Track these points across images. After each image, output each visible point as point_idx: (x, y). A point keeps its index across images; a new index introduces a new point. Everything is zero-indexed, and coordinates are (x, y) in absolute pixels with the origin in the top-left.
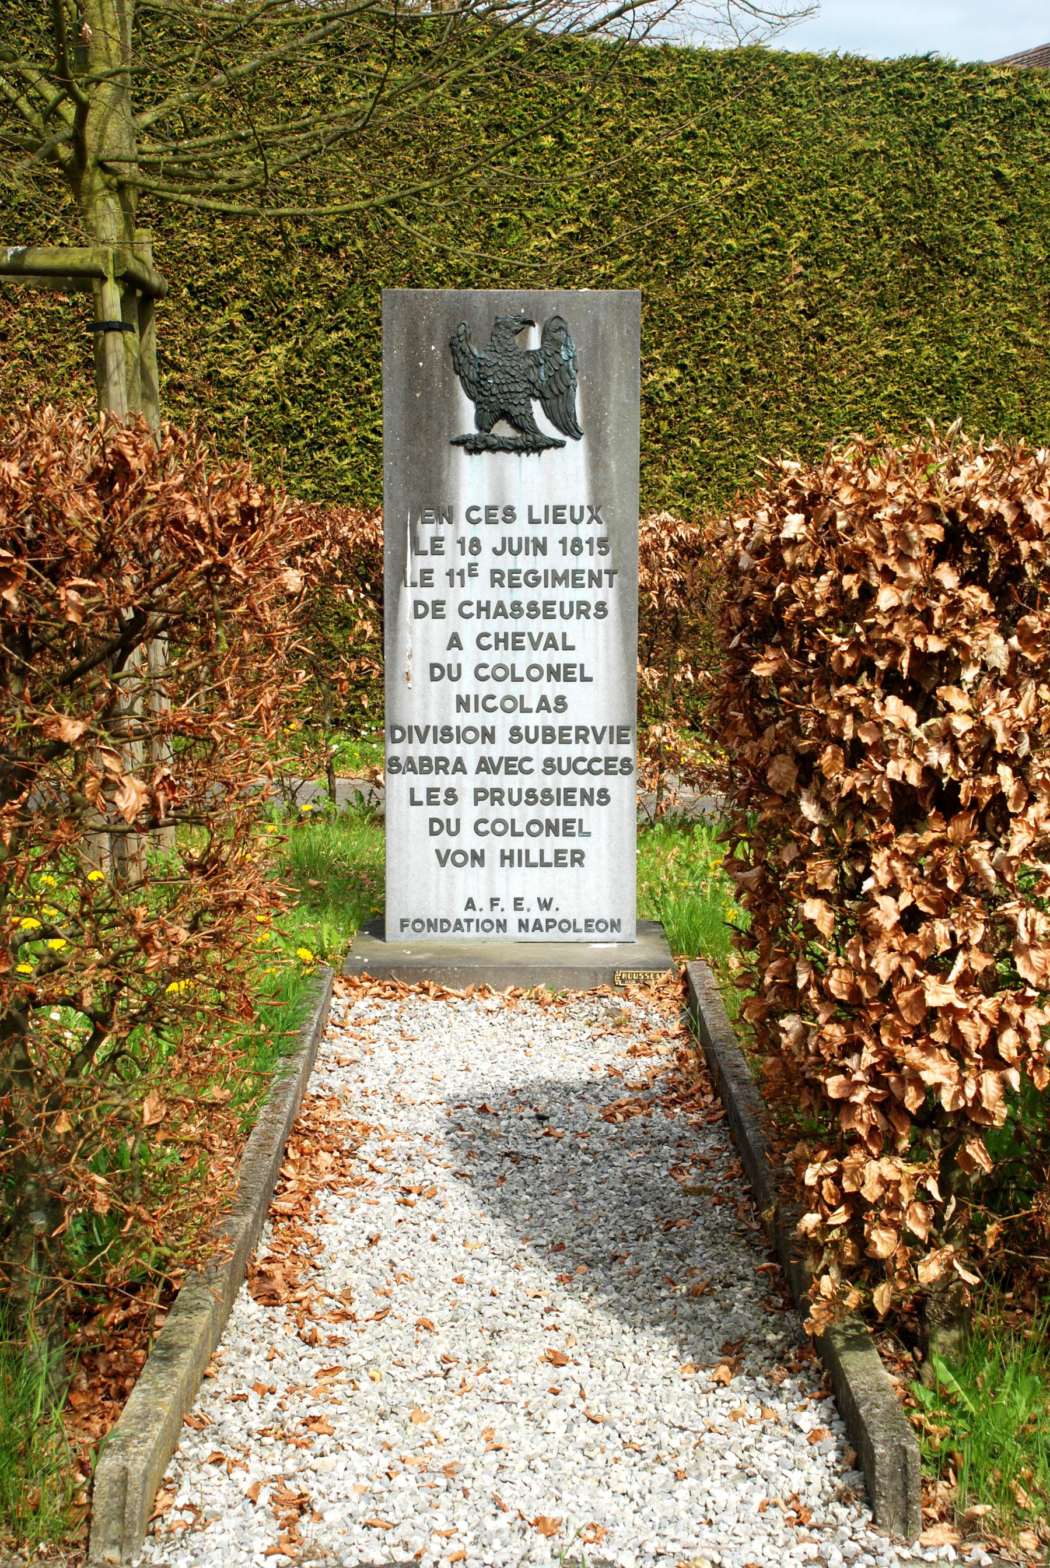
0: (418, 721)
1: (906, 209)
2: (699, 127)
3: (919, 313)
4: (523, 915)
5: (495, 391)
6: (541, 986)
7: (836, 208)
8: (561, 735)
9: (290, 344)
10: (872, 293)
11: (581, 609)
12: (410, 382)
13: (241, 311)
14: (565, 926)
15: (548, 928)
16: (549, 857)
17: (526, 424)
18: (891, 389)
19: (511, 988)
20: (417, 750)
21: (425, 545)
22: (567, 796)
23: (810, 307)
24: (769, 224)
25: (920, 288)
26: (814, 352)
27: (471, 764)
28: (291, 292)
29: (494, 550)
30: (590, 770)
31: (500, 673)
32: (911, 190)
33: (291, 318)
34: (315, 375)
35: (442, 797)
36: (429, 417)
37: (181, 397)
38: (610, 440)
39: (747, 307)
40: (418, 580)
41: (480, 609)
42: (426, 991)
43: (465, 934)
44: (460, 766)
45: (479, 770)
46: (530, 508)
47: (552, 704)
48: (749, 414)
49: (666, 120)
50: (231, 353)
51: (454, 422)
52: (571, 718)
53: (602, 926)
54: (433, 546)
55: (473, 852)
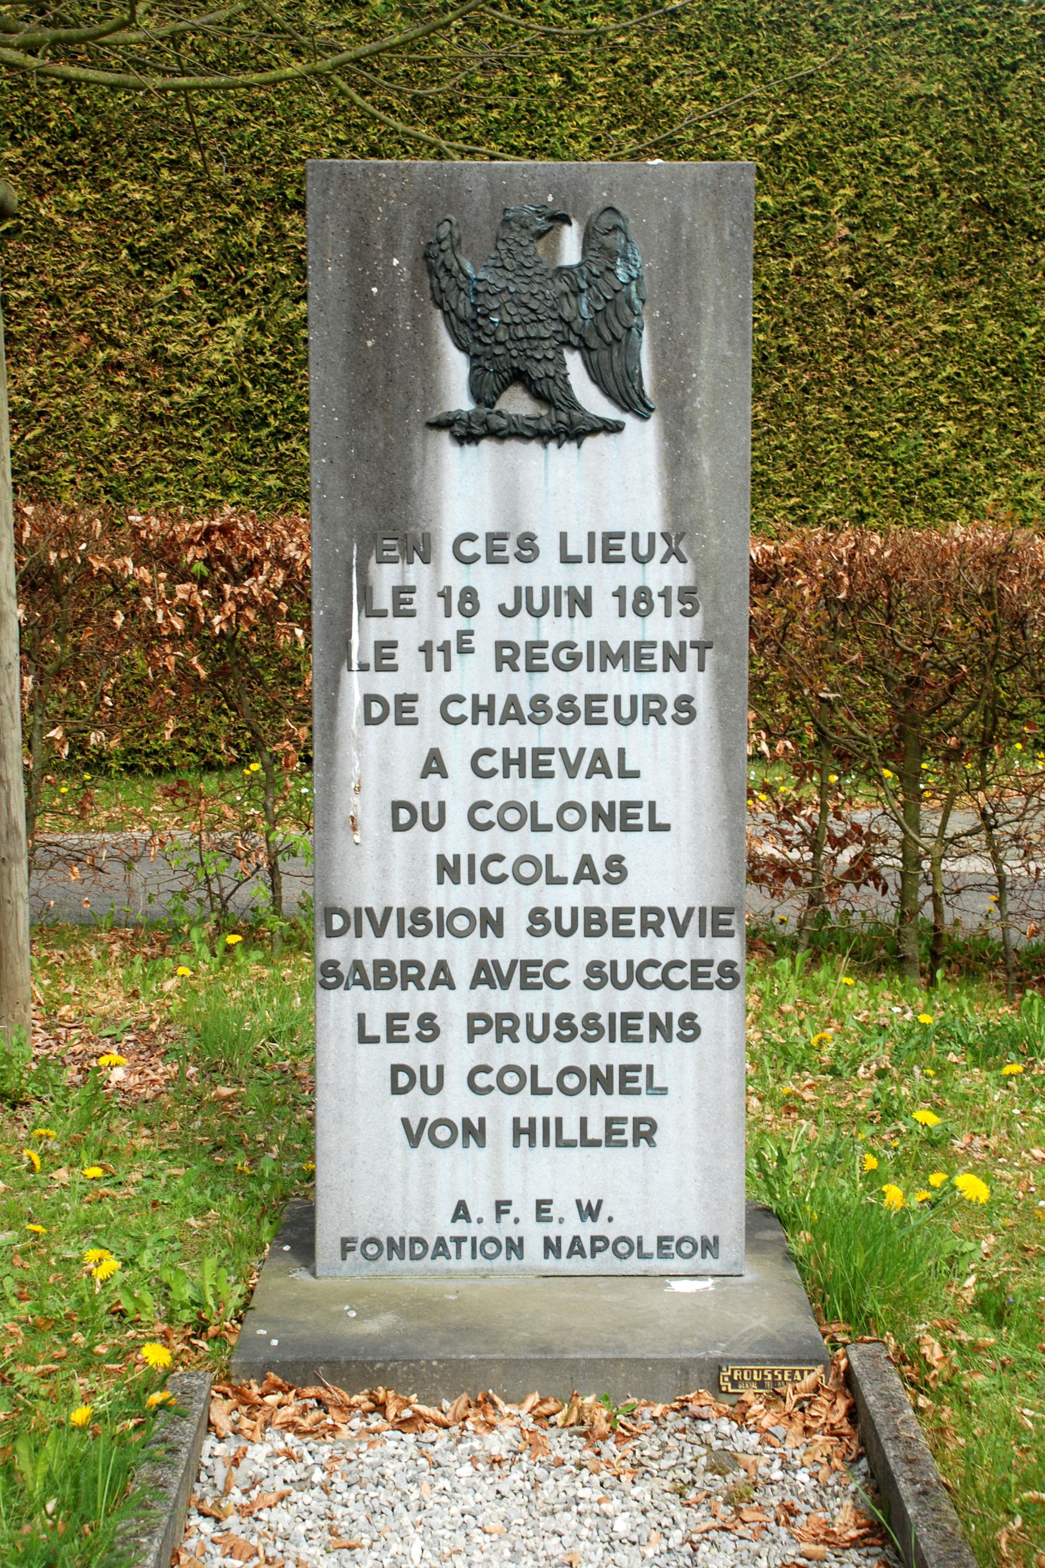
0: (370, 900)
1: (967, 164)
2: (730, 66)
3: (981, 282)
4: (552, 1230)
5: (502, 336)
6: (589, 1400)
7: (887, 161)
8: (617, 922)
9: (251, 316)
10: (928, 260)
11: (651, 709)
12: (355, 320)
13: (192, 277)
14: (623, 1248)
15: (594, 1251)
16: (597, 1131)
17: (556, 393)
18: (950, 370)
19: (533, 1399)
20: (369, 949)
21: (384, 600)
22: (626, 1026)
23: (857, 275)
24: (810, 179)
25: (983, 255)
26: (862, 327)
27: (462, 972)
28: (252, 255)
29: (502, 609)
30: (665, 981)
31: (512, 817)
32: (972, 141)
33: (251, 284)
34: (280, 352)
35: (412, 1028)
36: (389, 381)
37: (121, 378)
38: (702, 421)
39: (785, 274)
40: (371, 659)
41: (477, 708)
42: (380, 1407)
43: (453, 1263)
44: (443, 976)
45: (475, 982)
46: (563, 537)
47: (601, 870)
48: (788, 398)
49: (691, 58)
50: (180, 326)
51: (432, 390)
52: (633, 893)
53: (686, 1248)
54: (397, 602)
55: (466, 1122)
